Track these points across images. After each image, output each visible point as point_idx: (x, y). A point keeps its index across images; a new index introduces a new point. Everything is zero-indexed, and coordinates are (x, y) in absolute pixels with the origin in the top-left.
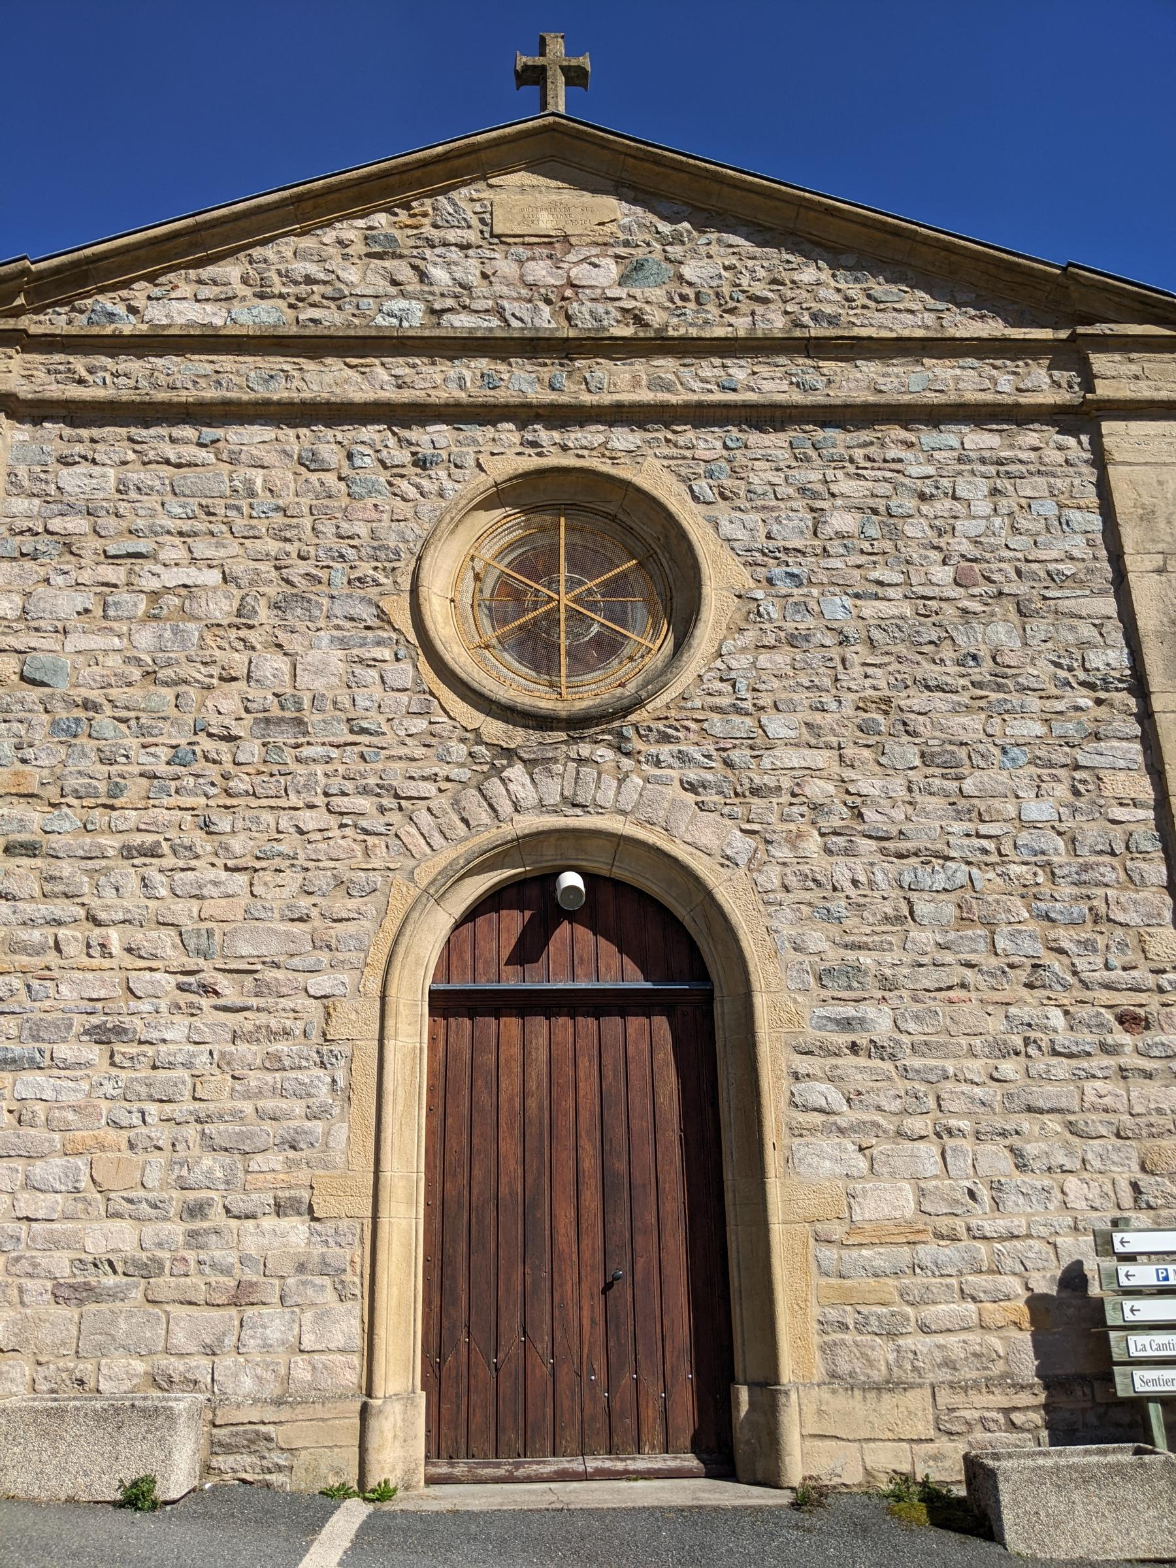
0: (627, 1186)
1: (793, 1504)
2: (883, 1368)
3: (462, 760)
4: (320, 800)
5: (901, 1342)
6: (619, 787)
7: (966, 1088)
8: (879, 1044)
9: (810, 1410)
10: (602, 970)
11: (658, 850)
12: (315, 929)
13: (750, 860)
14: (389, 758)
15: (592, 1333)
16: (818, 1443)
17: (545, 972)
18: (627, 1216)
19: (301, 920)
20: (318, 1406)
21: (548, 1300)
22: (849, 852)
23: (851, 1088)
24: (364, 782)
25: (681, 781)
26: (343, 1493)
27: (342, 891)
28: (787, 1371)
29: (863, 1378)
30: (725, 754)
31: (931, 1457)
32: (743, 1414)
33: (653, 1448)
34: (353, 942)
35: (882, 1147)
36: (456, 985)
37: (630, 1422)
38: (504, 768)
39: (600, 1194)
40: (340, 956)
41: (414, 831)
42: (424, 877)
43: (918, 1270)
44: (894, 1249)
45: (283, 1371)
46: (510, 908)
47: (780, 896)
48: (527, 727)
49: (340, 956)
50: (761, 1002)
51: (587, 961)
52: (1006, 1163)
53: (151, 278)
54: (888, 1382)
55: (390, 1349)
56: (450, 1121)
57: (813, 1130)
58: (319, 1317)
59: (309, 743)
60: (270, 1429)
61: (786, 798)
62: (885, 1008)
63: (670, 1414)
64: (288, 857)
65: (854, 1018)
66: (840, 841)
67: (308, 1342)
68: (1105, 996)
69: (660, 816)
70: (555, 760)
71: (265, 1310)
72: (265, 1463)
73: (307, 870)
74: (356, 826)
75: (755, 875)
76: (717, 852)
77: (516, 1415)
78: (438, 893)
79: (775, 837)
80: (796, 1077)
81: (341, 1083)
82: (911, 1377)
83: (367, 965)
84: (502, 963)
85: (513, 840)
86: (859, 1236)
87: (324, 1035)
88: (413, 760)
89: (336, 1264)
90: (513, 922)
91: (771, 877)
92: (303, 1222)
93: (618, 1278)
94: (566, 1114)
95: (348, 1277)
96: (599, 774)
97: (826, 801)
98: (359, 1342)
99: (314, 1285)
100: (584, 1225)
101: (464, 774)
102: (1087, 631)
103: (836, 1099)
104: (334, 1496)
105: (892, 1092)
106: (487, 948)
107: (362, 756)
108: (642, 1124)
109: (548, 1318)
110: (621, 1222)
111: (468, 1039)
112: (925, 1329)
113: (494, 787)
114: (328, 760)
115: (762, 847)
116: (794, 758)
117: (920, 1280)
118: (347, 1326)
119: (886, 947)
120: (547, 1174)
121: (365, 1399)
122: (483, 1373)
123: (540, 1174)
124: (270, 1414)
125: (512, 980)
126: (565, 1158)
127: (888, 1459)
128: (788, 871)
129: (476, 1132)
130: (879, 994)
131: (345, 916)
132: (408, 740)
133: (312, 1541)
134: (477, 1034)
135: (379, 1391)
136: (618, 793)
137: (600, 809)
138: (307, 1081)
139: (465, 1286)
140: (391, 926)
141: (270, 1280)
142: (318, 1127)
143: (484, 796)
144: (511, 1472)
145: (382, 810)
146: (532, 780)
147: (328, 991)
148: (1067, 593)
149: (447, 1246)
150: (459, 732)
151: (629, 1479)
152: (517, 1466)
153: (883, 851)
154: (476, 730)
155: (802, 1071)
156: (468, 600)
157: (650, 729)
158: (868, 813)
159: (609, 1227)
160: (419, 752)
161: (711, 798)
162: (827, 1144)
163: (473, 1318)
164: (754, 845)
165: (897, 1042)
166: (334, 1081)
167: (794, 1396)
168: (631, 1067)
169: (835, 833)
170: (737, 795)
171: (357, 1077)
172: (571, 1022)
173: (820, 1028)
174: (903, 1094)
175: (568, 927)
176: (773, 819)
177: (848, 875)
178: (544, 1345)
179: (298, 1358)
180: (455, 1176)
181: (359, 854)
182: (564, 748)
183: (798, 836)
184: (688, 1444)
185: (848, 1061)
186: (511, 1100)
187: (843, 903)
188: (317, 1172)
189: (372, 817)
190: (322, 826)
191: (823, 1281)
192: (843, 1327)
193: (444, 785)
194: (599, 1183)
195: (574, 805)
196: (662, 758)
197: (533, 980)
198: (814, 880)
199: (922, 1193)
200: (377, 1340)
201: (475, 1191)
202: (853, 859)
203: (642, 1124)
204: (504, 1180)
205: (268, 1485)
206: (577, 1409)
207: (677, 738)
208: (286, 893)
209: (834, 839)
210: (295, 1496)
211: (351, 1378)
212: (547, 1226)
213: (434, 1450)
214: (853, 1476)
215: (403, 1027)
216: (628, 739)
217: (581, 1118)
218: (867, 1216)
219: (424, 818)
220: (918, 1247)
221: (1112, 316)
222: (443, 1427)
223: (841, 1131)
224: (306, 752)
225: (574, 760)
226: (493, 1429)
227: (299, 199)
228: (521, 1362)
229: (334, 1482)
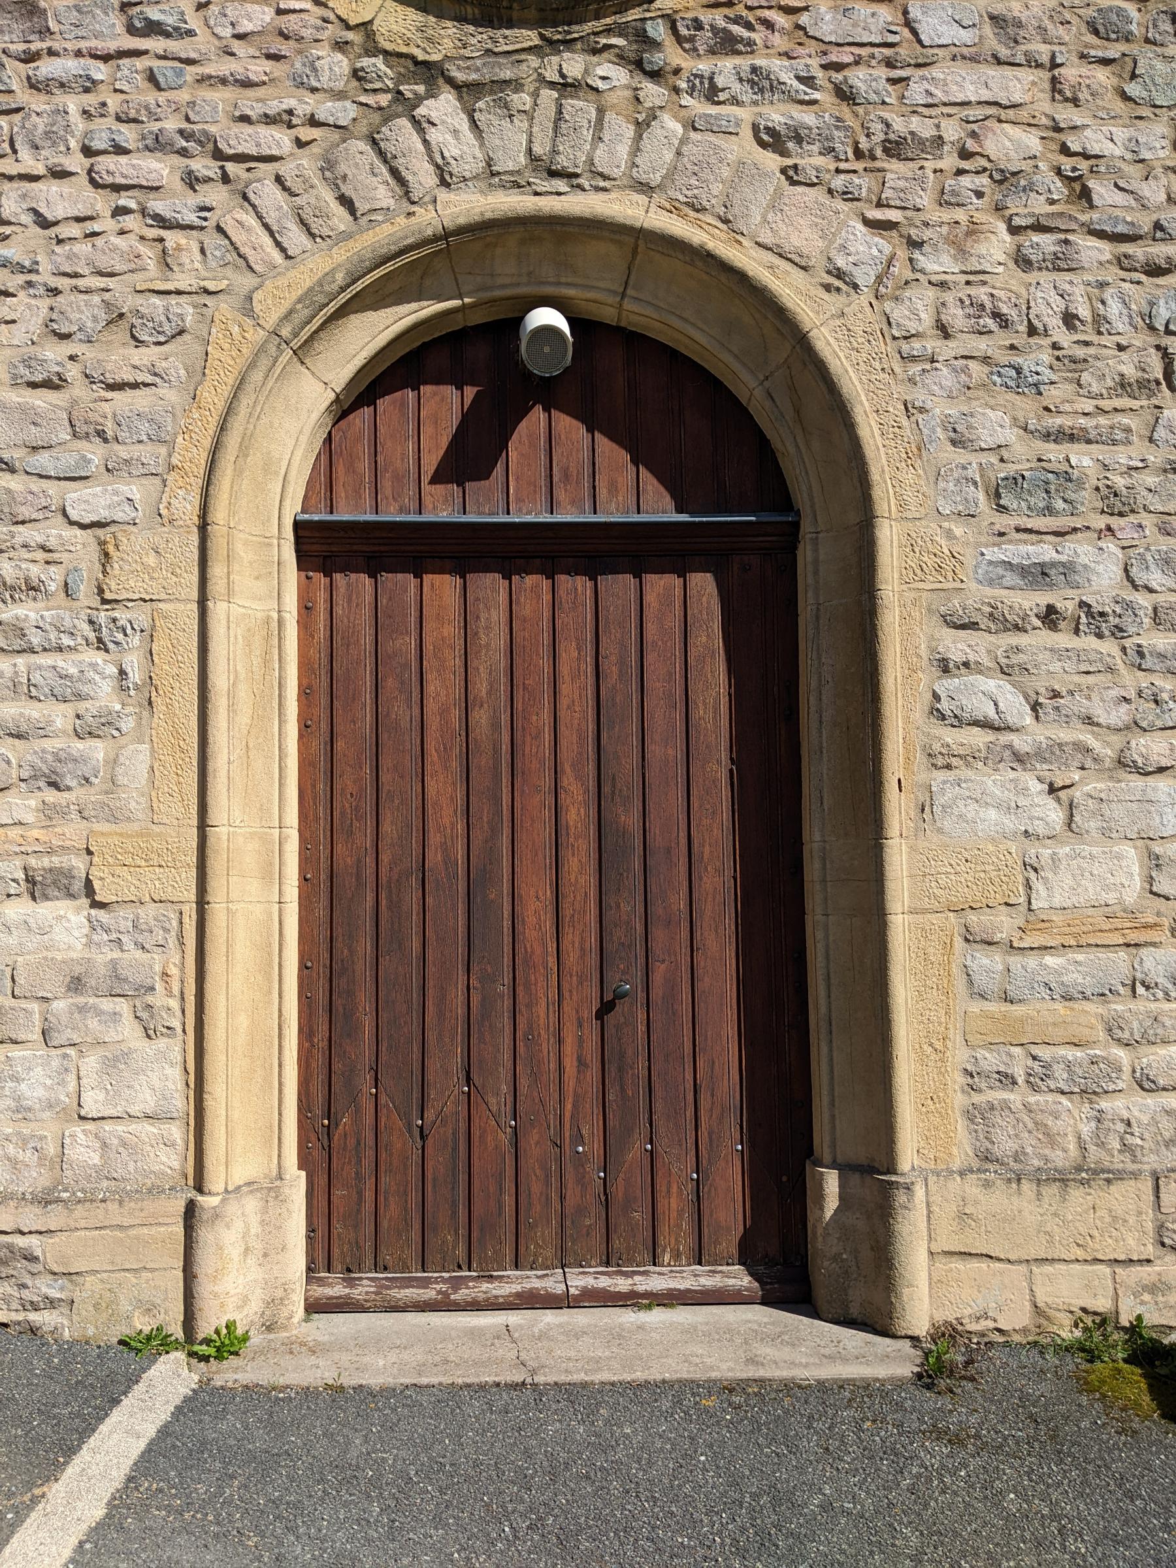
0: (639, 851)
1: (919, 1376)
2: (1072, 1147)
3: (340, 85)
4: (76, 163)
5: (1104, 1104)
6: (639, 137)
8: (1097, 608)
9: (946, 1212)
10: (603, 493)
11: (708, 257)
12: (74, 402)
13: (879, 280)
14: (202, 80)
15: (581, 1082)
16: (957, 1264)
17: (501, 496)
18: (640, 898)
19: (47, 384)
20: (112, 1207)
21: (508, 1030)
22: (1060, 264)
23: (1041, 685)
24: (155, 127)
25: (755, 128)
26: (154, 1344)
27: (120, 334)
28: (910, 1152)
29: (1036, 1163)
30: (838, 77)
31: (1145, 1288)
32: (829, 1213)
33: (677, 1256)
34: (144, 427)
35: (1089, 786)
36: (343, 515)
37: (640, 1216)
38: (419, 100)
39: (594, 863)
40: (123, 452)
41: (251, 220)
42: (273, 304)
43: (1140, 990)
44: (1102, 954)
45: (52, 1149)
46: (438, 380)
47: (932, 344)
48: (461, 19)
49: (123, 452)
50: (889, 537)
51: (570, 473)
54: (1079, 1169)
55: (236, 1115)
56: (340, 745)
57: (970, 758)
59: (51, 53)
60: (33, 1242)
61: (950, 161)
62: (1110, 546)
63: (705, 1205)
64: (21, 269)
65: (1053, 564)
66: (1047, 242)
67: (93, 1103)
69: (713, 192)
70: (516, 85)
71: (16, 1052)
72: (26, 1294)
73: (55, 292)
74: (143, 212)
75: (888, 306)
76: (818, 262)
77: (454, 1205)
79: (927, 234)
80: (945, 667)
81: (135, 676)
82: (1120, 1161)
83: (172, 468)
84: (425, 479)
85: (435, 239)
86: (1036, 933)
87: (101, 591)
88: (247, 84)
89: (137, 978)
90: (443, 407)
91: (916, 310)
92: (78, 910)
93: (624, 995)
94: (538, 736)
95: (158, 999)
96: (601, 111)
97: (1026, 166)
98: (180, 1103)
99: (99, 1013)
100: (567, 912)
101: (345, 112)
103: (1015, 707)
104: (144, 1348)
105: (1115, 693)
106: (399, 453)
107: (152, 78)
108: (665, 751)
109: (507, 1056)
110: (628, 907)
111: (367, 613)
112: (1145, 1084)
113: (401, 135)
114: (89, 86)
115: (902, 253)
116: (967, 84)
117: (1144, 1005)
118: (161, 1077)
119: (1119, 435)
120: (507, 831)
121: (192, 1194)
122: (401, 1142)
123: (495, 831)
124: (31, 1218)
125: (441, 508)
126: (536, 806)
127: (1073, 1292)
128: (949, 297)
129: (386, 762)
130: (1100, 522)
131: (128, 376)
132: (236, 46)
133: (35, 1501)
134: (383, 601)
135: (216, 1180)
136: (636, 150)
137: (602, 181)
138: (73, 671)
139: (369, 1008)
140: (214, 397)
141: (24, 1004)
142: (97, 750)
143: (381, 154)
144: (446, 1294)
145: (192, 181)
146: (474, 124)
147: (103, 514)
149: (338, 945)
150: (333, 31)
151: (641, 1307)
152: (457, 1283)
153: (1122, 262)
154: (365, 26)
155: (956, 656)
157: (698, 25)
158: (1102, 191)
159: (609, 915)
160: (258, 69)
161: (812, 161)
162: (994, 782)
163: (384, 1057)
164: (887, 249)
165: (1129, 606)
166: (122, 672)
167: (919, 1192)
168: (650, 658)
169: (1039, 228)
170: (859, 154)
171: (163, 666)
172: (546, 584)
173: (991, 583)
174: (1132, 694)
175: (543, 416)
176: (925, 200)
177: (1059, 304)
178: (498, 1098)
179: (78, 1129)
180: (350, 833)
181: (151, 265)
182: (534, 61)
183: (970, 233)
184: (734, 1251)
185: (1040, 639)
186: (444, 711)
187: (1046, 357)
188: (97, 827)
189: (174, 195)
190: (81, 210)
191: (976, 1007)
192: (1007, 1079)
193: (306, 133)
194: (594, 845)
195: (553, 174)
196: (720, 82)
197: (481, 506)
198: (996, 315)
199: (1155, 862)
200: (209, 1102)
201: (385, 858)
202: (1068, 276)
203: (665, 751)
204: (434, 839)
205: (33, 1330)
206: (554, 1196)
207: (750, 43)
208: (18, 335)
209: (1037, 238)
210: (73, 1350)
211: (168, 1157)
212: (507, 913)
213: (322, 1257)
214: (1015, 1318)
215: (244, 580)
216: (655, 45)
217: (564, 743)
218: (1057, 902)
219: (268, 195)
220: (1144, 952)
222: (334, 1222)
223: (1020, 759)
224: (47, 68)
225: (552, 85)
226: (417, 1226)
228: (463, 1126)
229: (143, 1324)
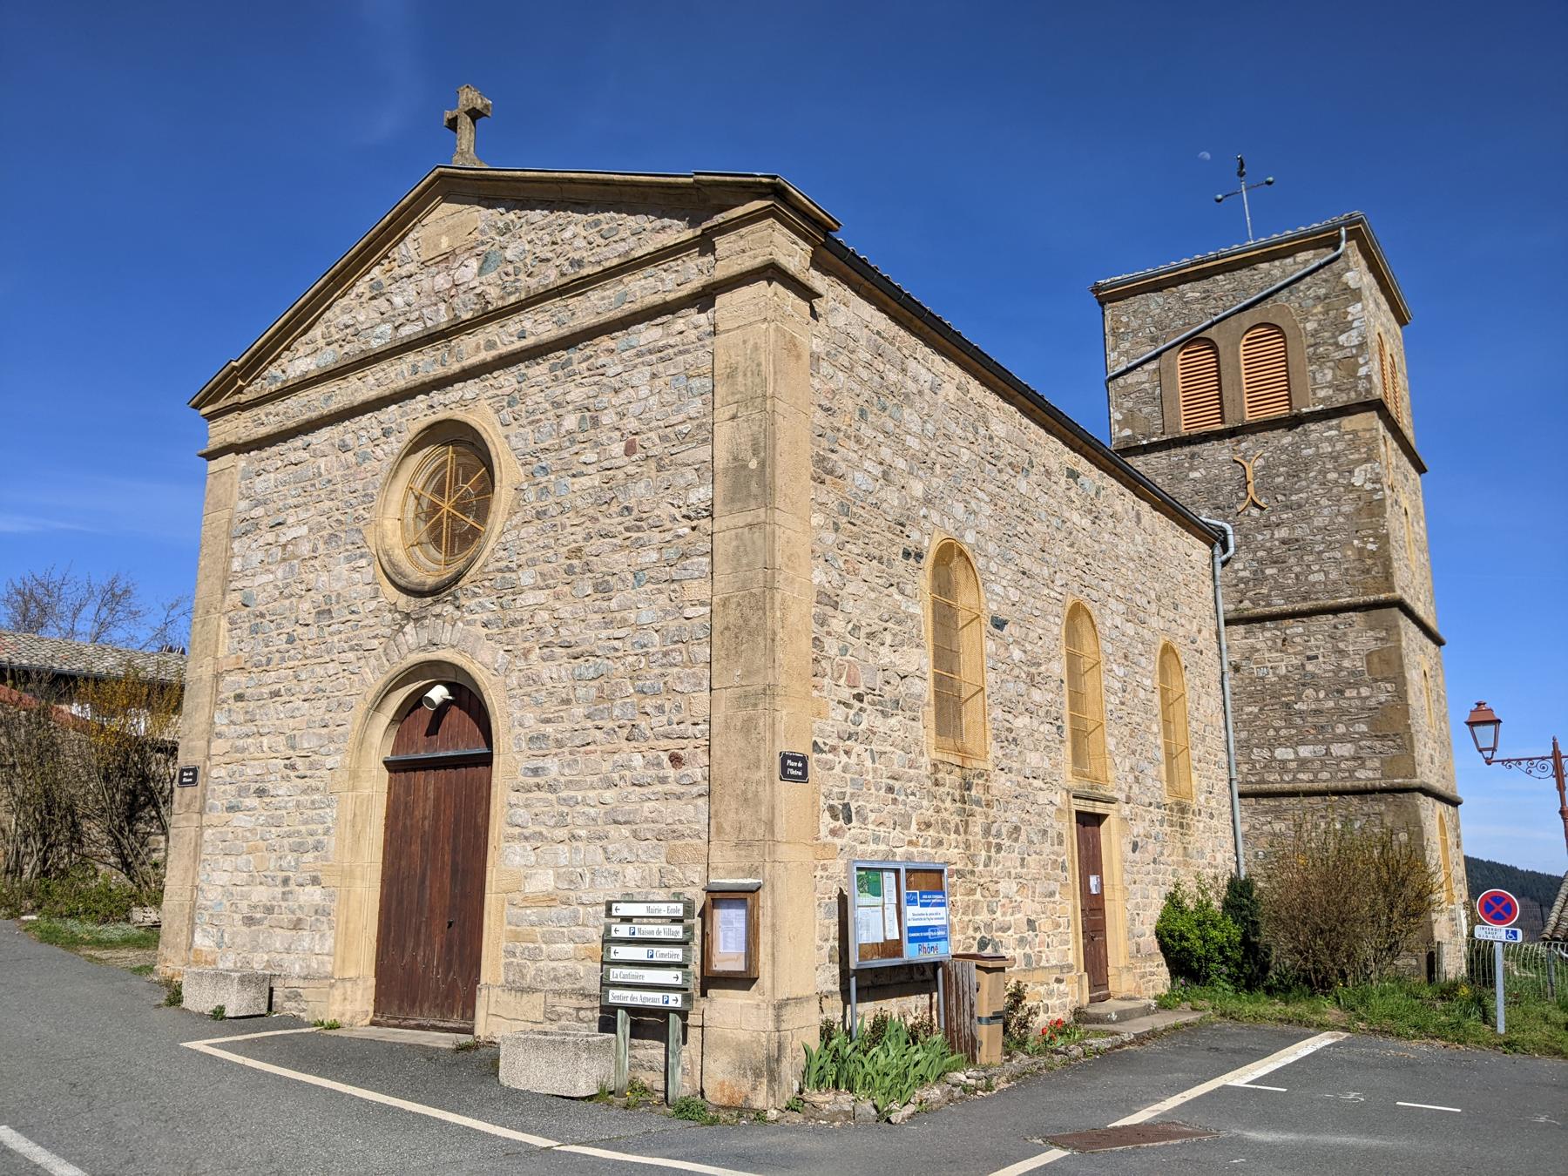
7: (586, 809)
52: (600, 857)
53: (288, 348)
58: (322, 936)
68: (664, 743)
78: (378, 706)
102: (691, 475)
124: (301, 983)
148: (683, 447)
156: (411, 515)
167: (484, 992)
221: (732, 201)
223: (526, 838)
227: (333, 278)
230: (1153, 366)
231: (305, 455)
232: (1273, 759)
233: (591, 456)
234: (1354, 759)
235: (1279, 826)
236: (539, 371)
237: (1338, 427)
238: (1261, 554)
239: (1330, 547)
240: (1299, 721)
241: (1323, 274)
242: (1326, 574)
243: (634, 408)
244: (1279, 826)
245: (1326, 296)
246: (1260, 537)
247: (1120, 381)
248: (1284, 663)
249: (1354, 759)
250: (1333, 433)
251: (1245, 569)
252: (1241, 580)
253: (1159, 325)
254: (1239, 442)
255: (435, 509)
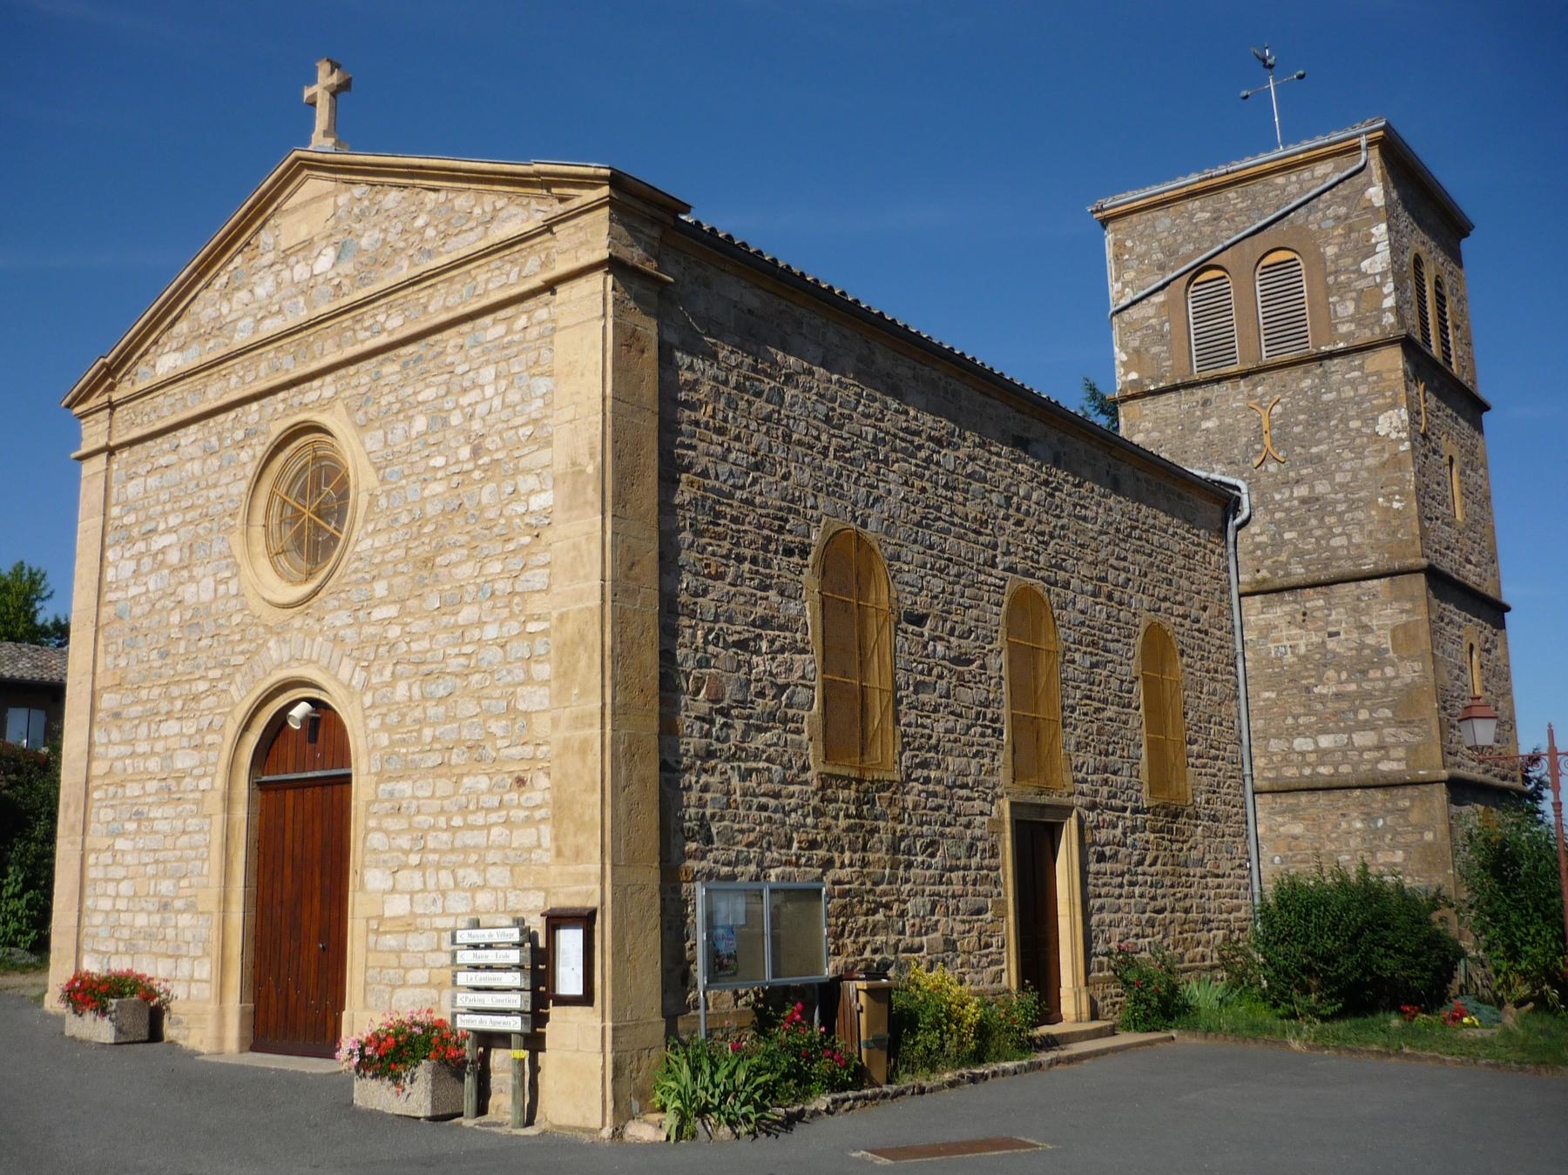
230: (1159, 298)
231: (172, 458)
232: (1291, 750)
233: (439, 461)
234: (1378, 748)
235: (1298, 829)
236: (390, 368)
237: (1361, 367)
238: (1278, 515)
239: (1352, 505)
240: (1319, 707)
241: (1342, 190)
242: (1349, 537)
243: (481, 409)
244: (1298, 829)
245: (1347, 217)
246: (1277, 497)
247: (1125, 315)
248: (1304, 640)
249: (1378, 748)
250: (1356, 374)
251: (1261, 534)
252: (1258, 546)
253: (1171, 252)
254: (1255, 386)
255: (297, 514)
